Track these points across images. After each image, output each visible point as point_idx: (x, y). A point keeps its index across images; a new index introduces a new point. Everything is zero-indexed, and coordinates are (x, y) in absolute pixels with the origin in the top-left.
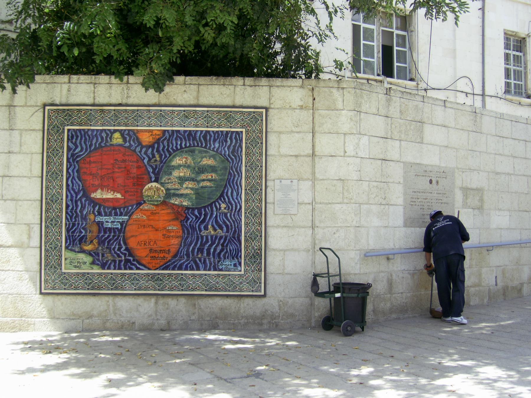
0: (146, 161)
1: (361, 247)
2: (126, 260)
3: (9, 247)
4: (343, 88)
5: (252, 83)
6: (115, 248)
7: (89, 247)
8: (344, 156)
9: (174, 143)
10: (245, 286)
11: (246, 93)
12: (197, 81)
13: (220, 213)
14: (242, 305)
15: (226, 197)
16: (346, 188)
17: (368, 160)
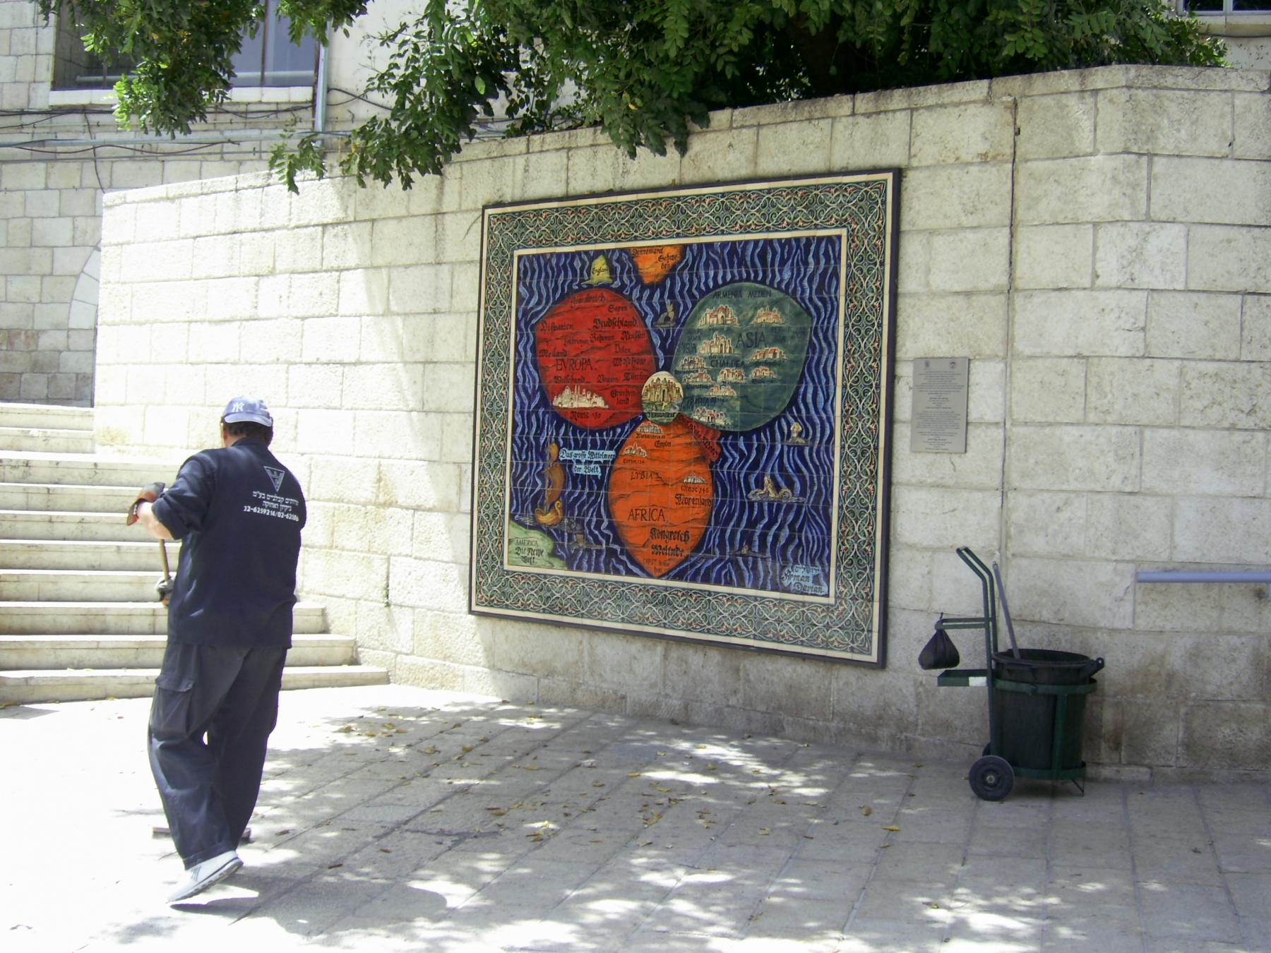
0: (649, 321)
1: (1139, 553)
2: (608, 549)
3: (430, 510)
4: (1095, 92)
5: (871, 107)
6: (590, 521)
7: (547, 519)
8: (1092, 289)
9: (702, 274)
10: (838, 635)
11: (857, 135)
12: (754, 117)
13: (789, 447)
14: (834, 685)
15: (802, 406)
16: (1094, 380)
17: (1180, 297)
